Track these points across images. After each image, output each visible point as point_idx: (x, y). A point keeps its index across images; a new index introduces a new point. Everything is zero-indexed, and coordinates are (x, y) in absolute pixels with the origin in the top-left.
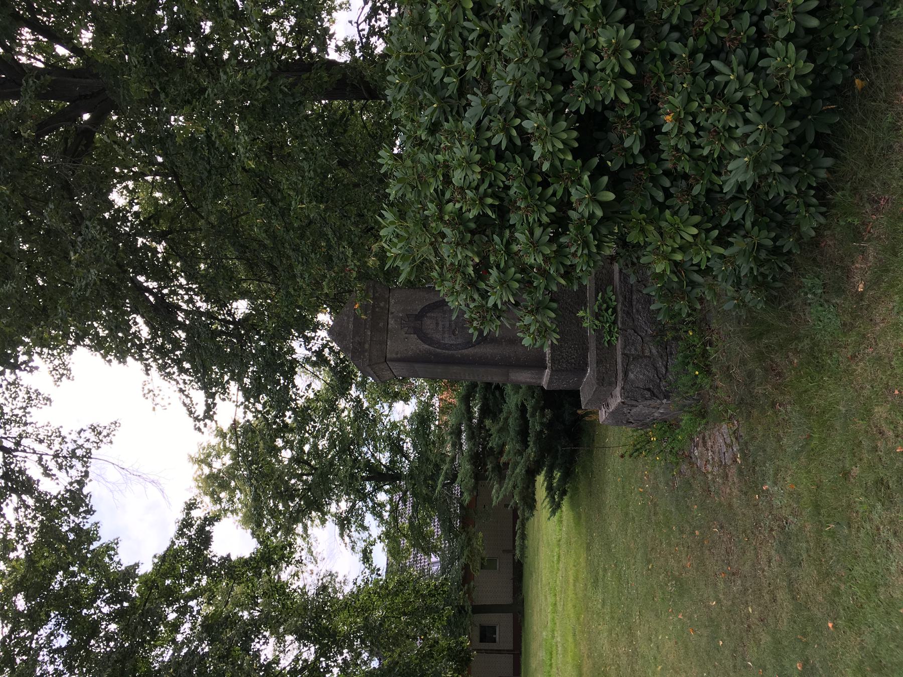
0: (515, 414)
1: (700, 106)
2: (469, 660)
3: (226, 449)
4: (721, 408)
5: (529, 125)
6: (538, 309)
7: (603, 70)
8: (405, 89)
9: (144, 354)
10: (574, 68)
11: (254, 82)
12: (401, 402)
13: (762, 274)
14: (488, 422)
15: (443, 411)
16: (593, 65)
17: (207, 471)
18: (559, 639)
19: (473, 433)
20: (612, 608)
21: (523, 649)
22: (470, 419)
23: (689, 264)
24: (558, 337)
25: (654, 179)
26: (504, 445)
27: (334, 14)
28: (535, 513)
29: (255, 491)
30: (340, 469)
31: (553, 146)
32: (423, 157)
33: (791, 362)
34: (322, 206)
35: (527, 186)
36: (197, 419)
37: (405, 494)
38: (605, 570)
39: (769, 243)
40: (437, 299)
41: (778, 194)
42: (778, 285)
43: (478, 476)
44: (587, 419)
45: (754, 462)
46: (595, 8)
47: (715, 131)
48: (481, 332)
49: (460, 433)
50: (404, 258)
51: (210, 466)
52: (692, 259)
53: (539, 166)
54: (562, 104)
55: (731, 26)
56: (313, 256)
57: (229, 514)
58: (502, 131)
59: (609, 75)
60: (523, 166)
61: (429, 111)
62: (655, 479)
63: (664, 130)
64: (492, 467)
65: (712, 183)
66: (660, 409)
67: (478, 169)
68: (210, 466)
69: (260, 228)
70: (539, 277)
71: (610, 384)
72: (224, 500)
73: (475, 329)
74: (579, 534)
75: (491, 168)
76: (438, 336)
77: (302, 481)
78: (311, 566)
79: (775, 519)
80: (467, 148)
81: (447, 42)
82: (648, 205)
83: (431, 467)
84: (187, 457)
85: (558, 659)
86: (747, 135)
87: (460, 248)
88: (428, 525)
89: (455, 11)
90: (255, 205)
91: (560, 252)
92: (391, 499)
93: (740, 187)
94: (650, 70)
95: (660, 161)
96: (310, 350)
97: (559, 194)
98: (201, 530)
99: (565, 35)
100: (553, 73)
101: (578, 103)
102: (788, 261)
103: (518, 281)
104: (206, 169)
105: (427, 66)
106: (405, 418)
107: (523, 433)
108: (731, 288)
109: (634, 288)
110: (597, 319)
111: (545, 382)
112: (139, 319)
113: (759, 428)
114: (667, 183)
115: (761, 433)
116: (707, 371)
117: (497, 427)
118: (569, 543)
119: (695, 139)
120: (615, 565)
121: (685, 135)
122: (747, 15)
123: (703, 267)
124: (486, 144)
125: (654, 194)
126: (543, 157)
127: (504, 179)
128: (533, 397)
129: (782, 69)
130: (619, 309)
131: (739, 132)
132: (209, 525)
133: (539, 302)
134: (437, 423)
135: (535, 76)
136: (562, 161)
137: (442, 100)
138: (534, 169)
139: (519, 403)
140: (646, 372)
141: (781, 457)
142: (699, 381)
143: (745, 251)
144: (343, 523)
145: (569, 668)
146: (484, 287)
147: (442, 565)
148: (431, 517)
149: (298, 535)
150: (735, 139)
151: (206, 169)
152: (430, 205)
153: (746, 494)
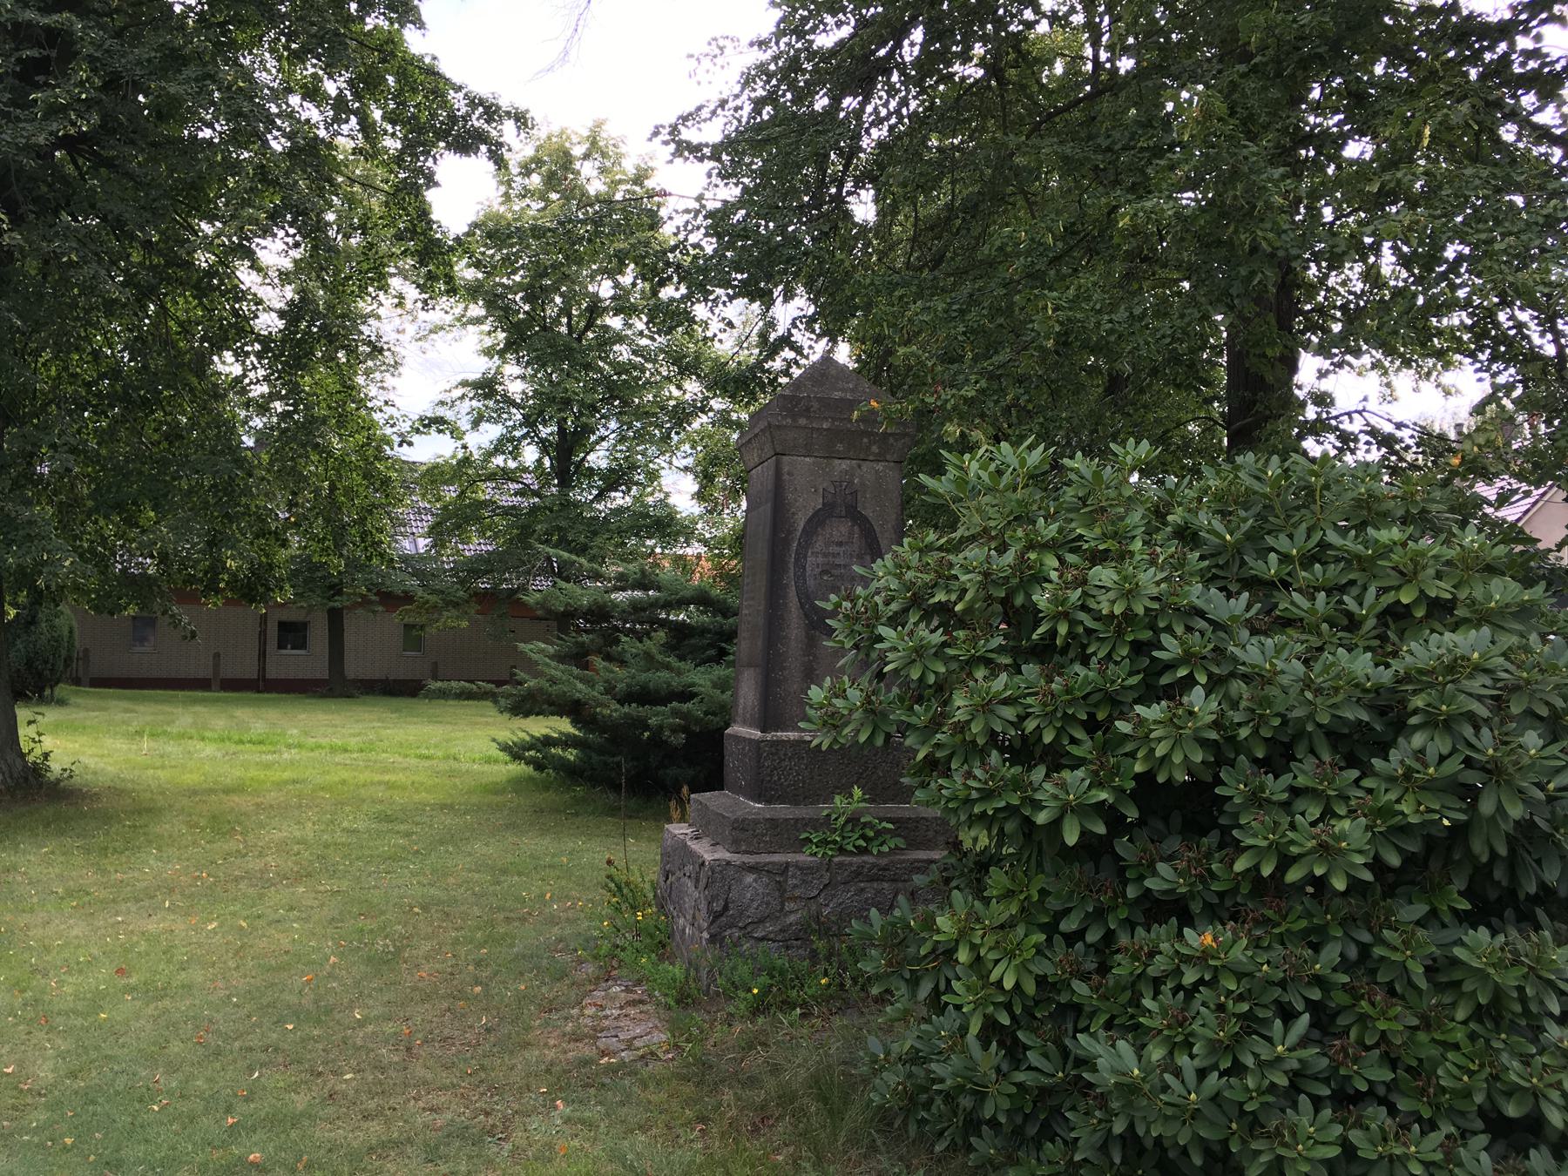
0: (676, 682)
1: (1229, 993)
2: (252, 600)
3: (615, 184)
4: (695, 1031)
5: (1196, 698)
6: (873, 713)
7: (1293, 827)
8: (1256, 486)
9: (786, 39)
10: (1295, 777)
11: (1268, 225)
12: (696, 488)
13: (931, 1101)
14: (661, 635)
15: (679, 560)
16: (1301, 809)
17: (578, 151)
18: (286, 756)
19: (644, 610)
20: (343, 844)
21: (266, 695)
22: (668, 606)
23: (950, 975)
24: (824, 748)
25: (1100, 914)
26: (623, 663)
27: (1374, 376)
28: (506, 716)
29: (550, 230)
30: (578, 381)
31: (1159, 740)
32: (1136, 517)
33: (777, 1151)
34: (1050, 344)
35: (1089, 694)
36: (674, 130)
37: (536, 494)
38: (408, 834)
39: (988, 1114)
40: (883, 543)
41: (1073, 1129)
42: (912, 1129)
43: (563, 619)
44: (673, 804)
45: (603, 1085)
46: (1402, 813)
47: (1185, 1019)
48: (833, 614)
49: (645, 588)
50: (961, 482)
51: (586, 156)
52: (959, 979)
53: (1123, 716)
54: (1232, 756)
55: (1368, 1049)
56: (961, 329)
57: (503, 189)
58: (1184, 651)
59: (1284, 835)
60: (1123, 687)
61: (1218, 525)
62: (568, 919)
63: (1186, 931)
64: (583, 643)
65: (1093, 1015)
66: (691, 927)
67: (1118, 610)
68: (586, 156)
69: (1010, 237)
70: (930, 715)
71: (736, 842)
72: (527, 181)
73: (838, 605)
74: (469, 792)
75: (1120, 633)
76: (819, 545)
77: (559, 316)
78: (411, 330)
79: (506, 1121)
80: (1154, 591)
81: (1337, 560)
82: (1054, 904)
83: (582, 539)
84: (603, 117)
85: (251, 754)
86: (1178, 1073)
87: (979, 578)
88: (482, 534)
89: (1393, 573)
90: (1050, 230)
91: (973, 751)
92: (525, 470)
93: (1087, 1063)
94: (1291, 908)
95: (1130, 925)
96: (794, 325)
97: (1075, 751)
98: (480, 137)
99: (1352, 761)
100: (1286, 740)
101: (1234, 784)
102: (953, 1147)
103: (922, 679)
104: (1114, 143)
105: (1295, 526)
106: (667, 495)
107: (645, 696)
108: (907, 1047)
109: (900, 885)
110: (847, 822)
111: (737, 729)
112: (846, 31)
113: (663, 1096)
114: (1093, 936)
115: (654, 1098)
116: (759, 1008)
117: (654, 651)
118: (452, 774)
119: (1170, 985)
120: (417, 852)
121: (1178, 967)
122: (1388, 1076)
123: (944, 998)
124: (1162, 625)
125: (1073, 915)
126: (1141, 722)
127: (1101, 654)
128: (706, 713)
129: (1294, 1134)
130: (865, 858)
131: (1183, 1060)
132: (490, 151)
133: (884, 715)
134: (658, 550)
135: (1281, 710)
136: (1132, 755)
137: (1238, 550)
138: (1117, 704)
139: (695, 689)
140: (755, 904)
141: (613, 1131)
142: (741, 994)
143: (975, 1070)
144: (486, 387)
145: (238, 773)
146: (912, 620)
147: (412, 557)
148: (496, 536)
149: (466, 309)
150: (1171, 1053)
151: (1114, 143)
152: (1054, 527)
153: (548, 1071)
